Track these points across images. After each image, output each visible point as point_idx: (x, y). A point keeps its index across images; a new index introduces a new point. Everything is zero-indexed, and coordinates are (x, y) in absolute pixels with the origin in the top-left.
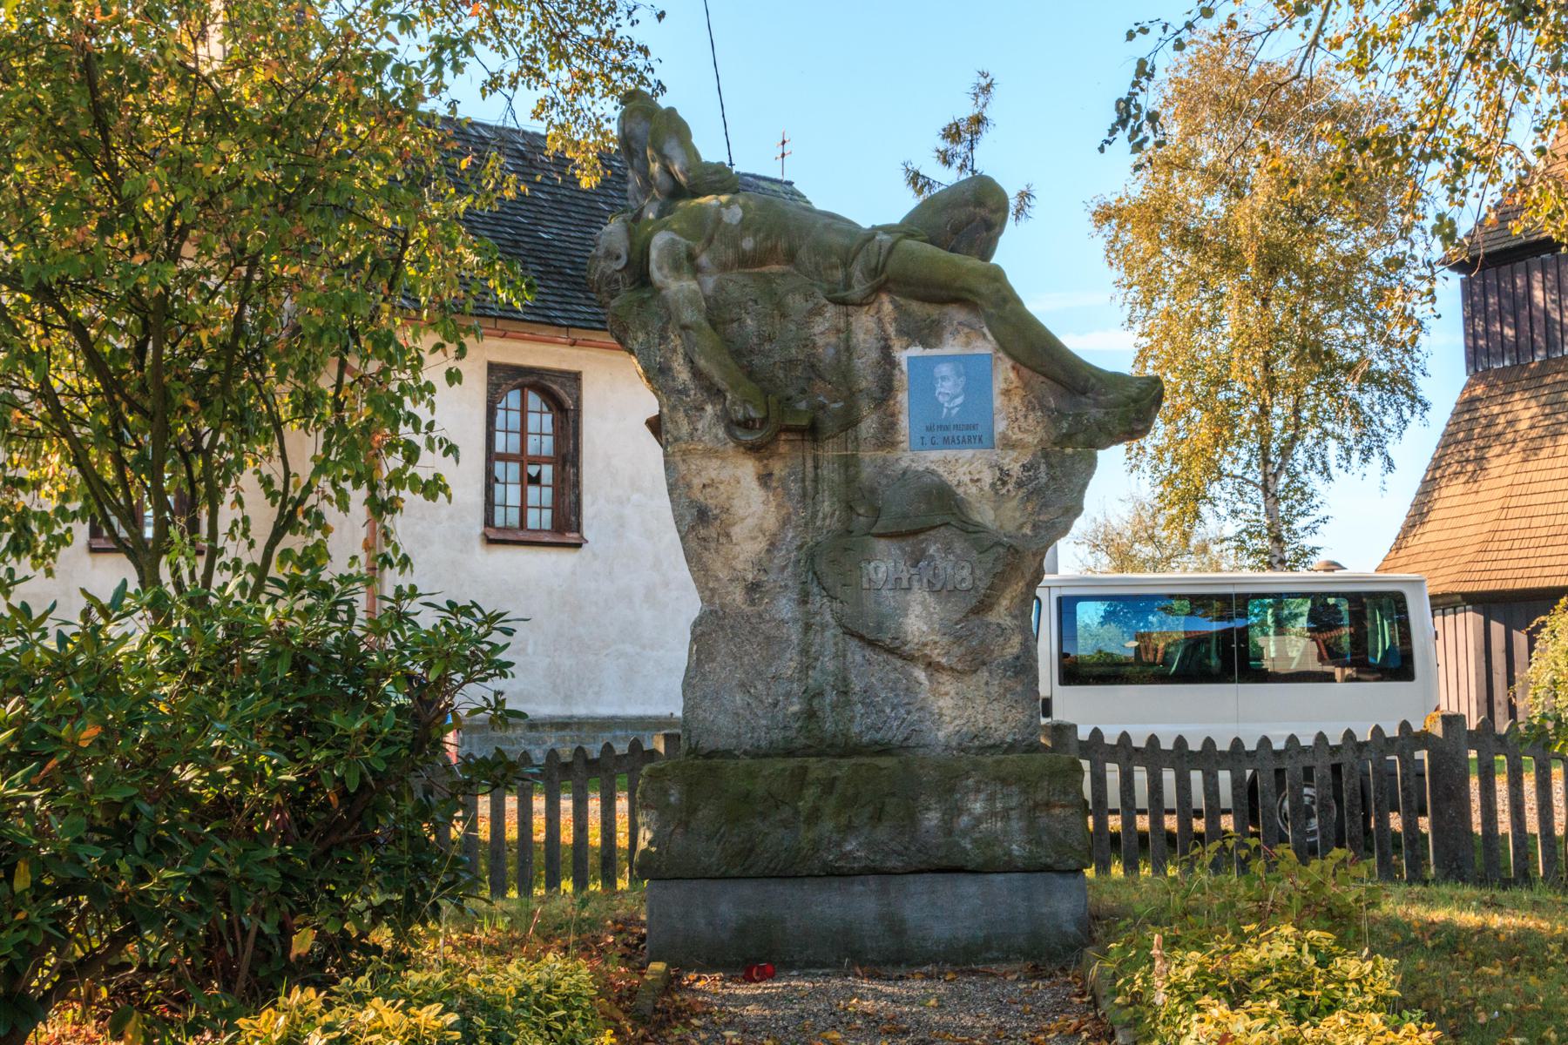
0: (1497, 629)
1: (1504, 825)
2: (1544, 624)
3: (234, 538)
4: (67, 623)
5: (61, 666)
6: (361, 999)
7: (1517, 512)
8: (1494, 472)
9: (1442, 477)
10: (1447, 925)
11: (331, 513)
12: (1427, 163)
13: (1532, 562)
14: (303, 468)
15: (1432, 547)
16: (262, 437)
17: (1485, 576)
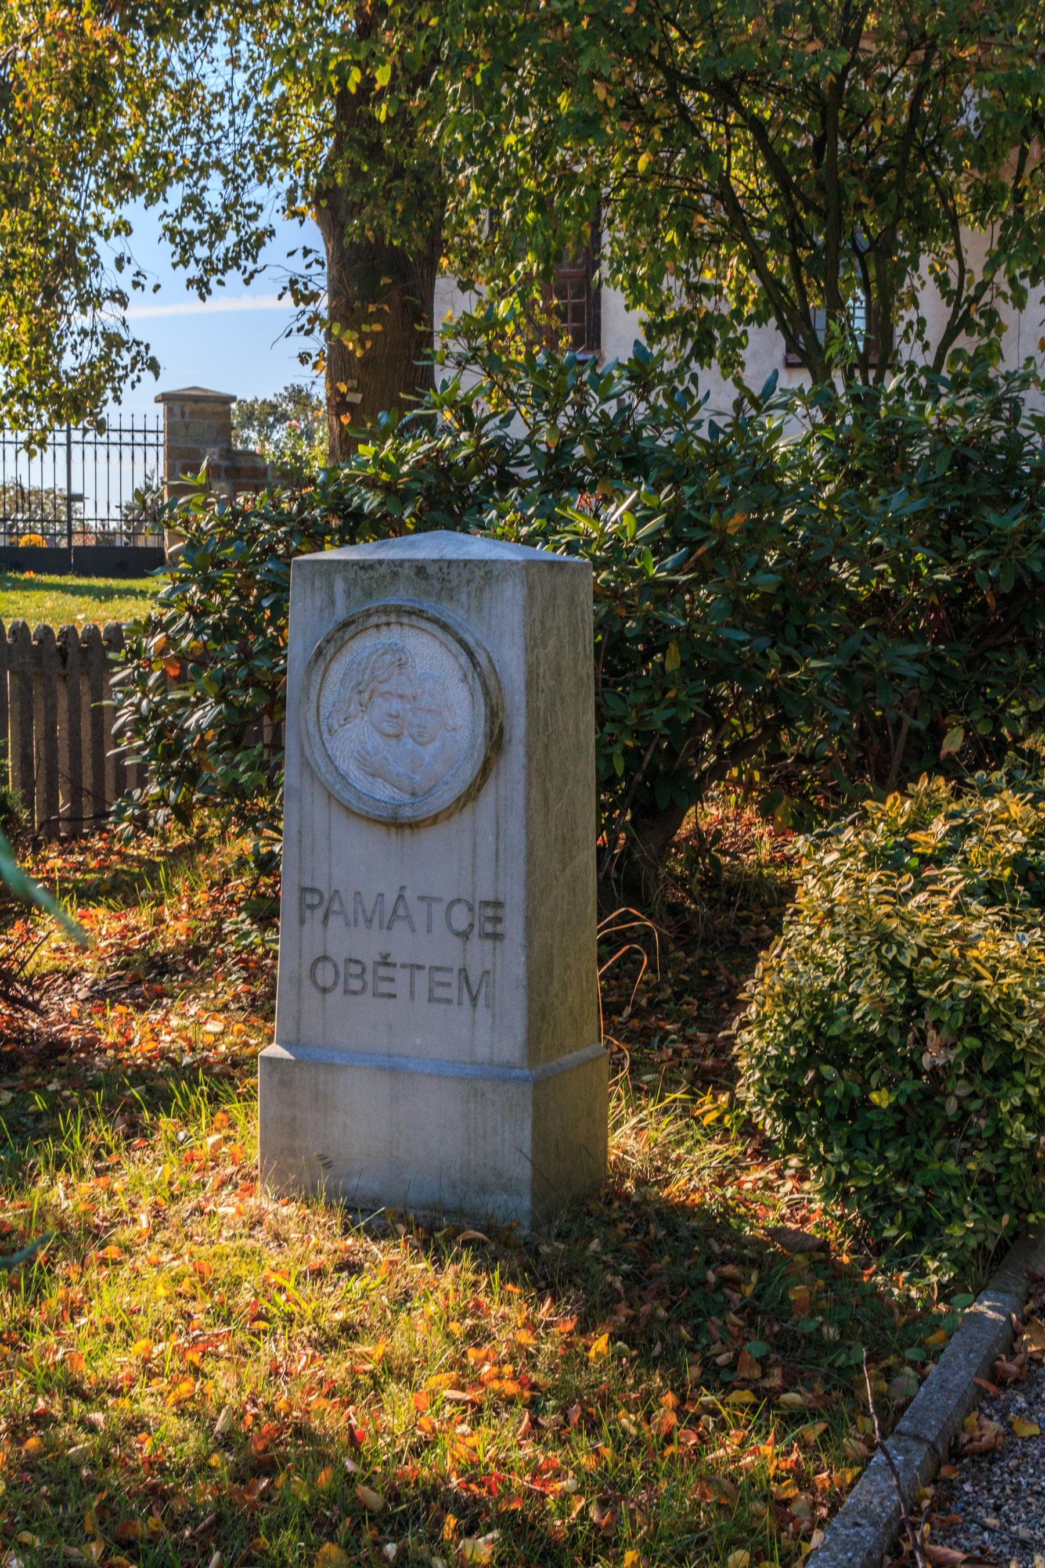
3: (908, 341)
4: (720, 414)
5: (717, 457)
6: (989, 791)
11: (1006, 312)
14: (976, 263)
16: (940, 234)
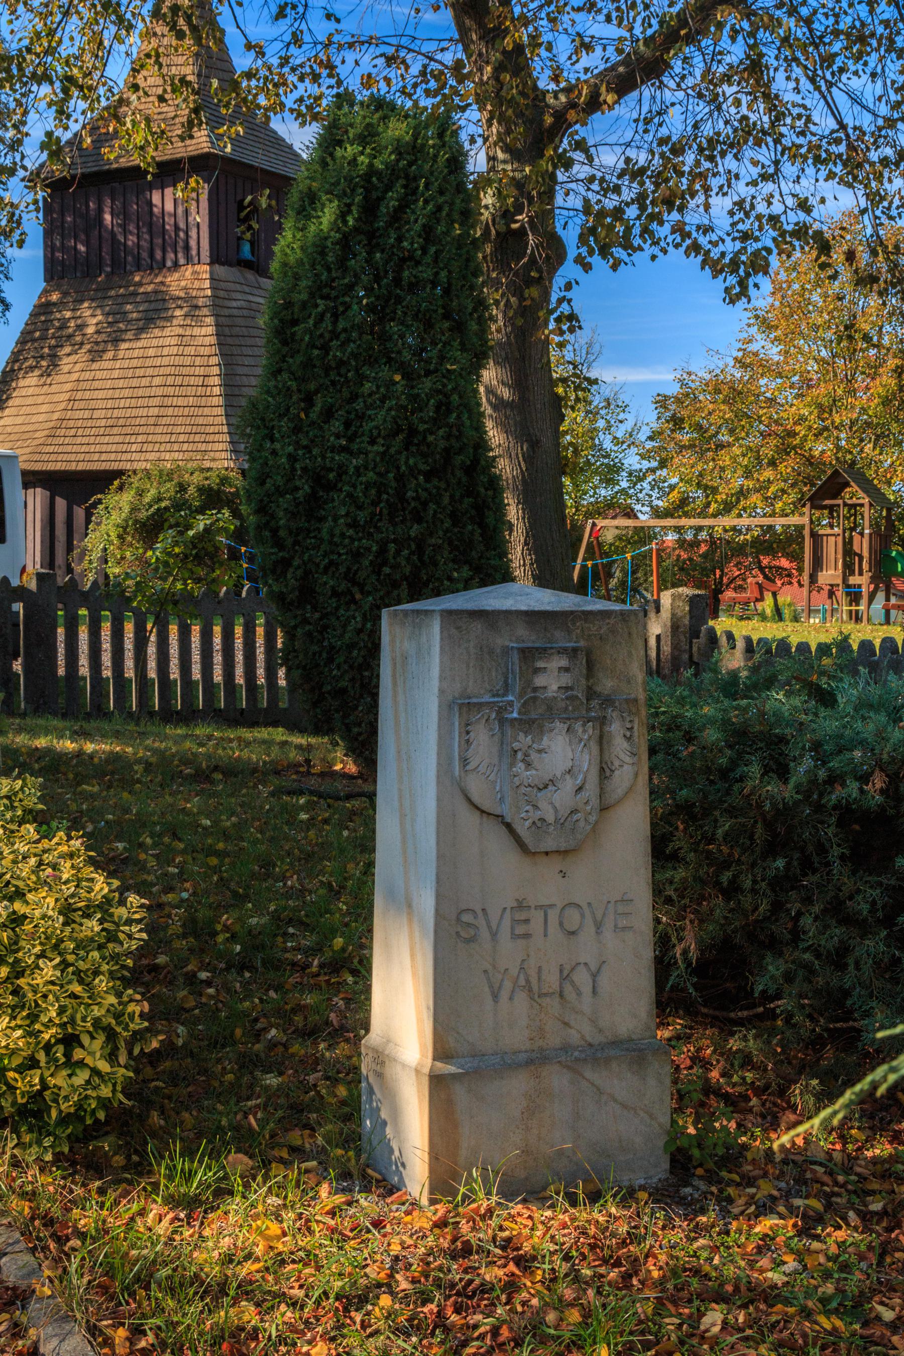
0: (61, 504)
1: (84, 670)
2: (100, 502)
7: (82, 405)
8: (66, 369)
9: (20, 369)
10: (49, 751)
12: (39, 84)
13: (92, 448)
15: (9, 429)
17: (53, 457)
